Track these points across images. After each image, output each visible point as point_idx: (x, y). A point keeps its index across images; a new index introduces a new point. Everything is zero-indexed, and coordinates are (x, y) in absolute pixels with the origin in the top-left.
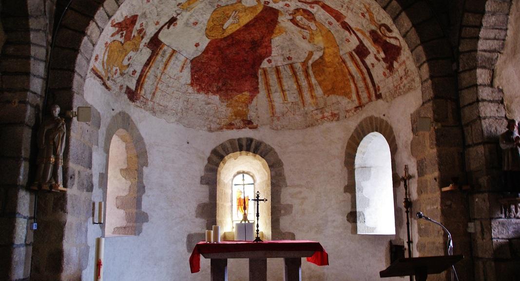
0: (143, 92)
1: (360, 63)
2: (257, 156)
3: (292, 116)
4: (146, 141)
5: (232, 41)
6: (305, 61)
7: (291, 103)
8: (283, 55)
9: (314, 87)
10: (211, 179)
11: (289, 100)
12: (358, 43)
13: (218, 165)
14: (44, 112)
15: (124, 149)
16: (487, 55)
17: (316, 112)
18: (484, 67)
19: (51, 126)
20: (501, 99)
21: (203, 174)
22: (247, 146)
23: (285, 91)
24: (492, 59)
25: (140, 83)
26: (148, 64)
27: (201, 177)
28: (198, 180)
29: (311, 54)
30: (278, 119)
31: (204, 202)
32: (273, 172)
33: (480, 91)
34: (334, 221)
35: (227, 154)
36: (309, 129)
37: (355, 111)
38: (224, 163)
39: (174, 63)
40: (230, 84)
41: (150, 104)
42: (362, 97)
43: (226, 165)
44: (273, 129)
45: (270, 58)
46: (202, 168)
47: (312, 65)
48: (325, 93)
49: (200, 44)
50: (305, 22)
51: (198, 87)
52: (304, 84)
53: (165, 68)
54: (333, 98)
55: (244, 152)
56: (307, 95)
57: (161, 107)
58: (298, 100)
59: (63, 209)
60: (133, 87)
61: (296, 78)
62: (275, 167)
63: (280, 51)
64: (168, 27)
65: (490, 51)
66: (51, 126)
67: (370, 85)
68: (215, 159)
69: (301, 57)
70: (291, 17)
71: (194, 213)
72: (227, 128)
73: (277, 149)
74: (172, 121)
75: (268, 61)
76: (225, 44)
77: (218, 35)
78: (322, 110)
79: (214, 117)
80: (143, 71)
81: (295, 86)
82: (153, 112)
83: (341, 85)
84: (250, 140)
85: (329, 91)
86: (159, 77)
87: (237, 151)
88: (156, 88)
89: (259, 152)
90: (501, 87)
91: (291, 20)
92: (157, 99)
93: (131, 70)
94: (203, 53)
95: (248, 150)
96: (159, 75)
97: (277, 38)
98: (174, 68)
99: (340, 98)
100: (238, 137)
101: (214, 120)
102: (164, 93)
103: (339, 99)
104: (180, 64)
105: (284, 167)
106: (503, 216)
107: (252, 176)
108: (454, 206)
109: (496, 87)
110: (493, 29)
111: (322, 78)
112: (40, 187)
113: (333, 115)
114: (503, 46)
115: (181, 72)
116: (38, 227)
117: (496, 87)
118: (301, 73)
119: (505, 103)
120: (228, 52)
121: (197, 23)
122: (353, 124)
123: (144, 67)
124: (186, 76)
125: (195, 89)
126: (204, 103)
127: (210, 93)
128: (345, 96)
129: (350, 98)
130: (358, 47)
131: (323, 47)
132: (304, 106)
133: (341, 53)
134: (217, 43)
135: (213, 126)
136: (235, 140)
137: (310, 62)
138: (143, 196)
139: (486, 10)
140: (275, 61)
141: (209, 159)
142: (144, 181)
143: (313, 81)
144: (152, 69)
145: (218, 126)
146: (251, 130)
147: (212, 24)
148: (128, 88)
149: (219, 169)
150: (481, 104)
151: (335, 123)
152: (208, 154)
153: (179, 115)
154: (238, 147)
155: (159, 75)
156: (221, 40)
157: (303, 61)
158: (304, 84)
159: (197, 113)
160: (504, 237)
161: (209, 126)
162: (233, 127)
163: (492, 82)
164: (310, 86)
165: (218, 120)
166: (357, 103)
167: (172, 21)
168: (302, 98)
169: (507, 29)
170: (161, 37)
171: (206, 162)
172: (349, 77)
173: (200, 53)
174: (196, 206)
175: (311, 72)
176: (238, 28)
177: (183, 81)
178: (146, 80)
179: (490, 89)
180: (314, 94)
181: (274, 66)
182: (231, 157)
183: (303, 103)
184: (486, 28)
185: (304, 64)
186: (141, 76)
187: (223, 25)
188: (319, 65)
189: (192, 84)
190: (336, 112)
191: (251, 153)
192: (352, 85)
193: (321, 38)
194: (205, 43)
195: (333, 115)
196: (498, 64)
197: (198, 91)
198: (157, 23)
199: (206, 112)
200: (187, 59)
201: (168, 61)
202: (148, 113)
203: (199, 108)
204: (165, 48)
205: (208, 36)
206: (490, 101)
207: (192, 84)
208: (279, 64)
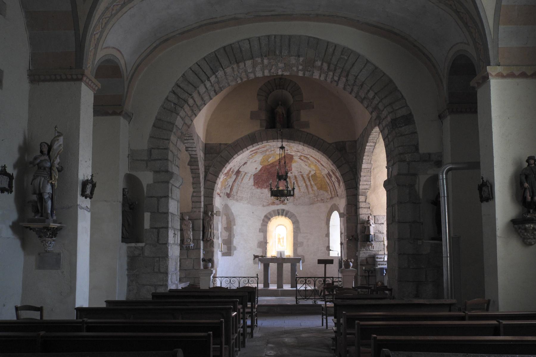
0: (233, 193)
1: (330, 179)
2: (287, 218)
4: (234, 214)
5: (273, 165)
6: (308, 174)
7: (303, 193)
8: (298, 171)
10: (264, 230)
11: (302, 191)
13: (267, 223)
14: (205, 213)
16: (364, 190)
18: (363, 195)
19: (209, 219)
20: (369, 207)
21: (260, 227)
22: (282, 213)
23: (299, 187)
24: (366, 192)
25: (231, 189)
28: (258, 230)
29: (310, 172)
31: (261, 240)
33: (361, 204)
37: (330, 199)
38: (270, 222)
39: (246, 178)
40: (273, 184)
41: (236, 197)
42: (332, 194)
43: (271, 222)
44: (294, 205)
45: (291, 171)
46: (260, 224)
48: (318, 189)
49: (258, 168)
50: (305, 159)
51: (257, 186)
52: (308, 184)
53: (242, 181)
54: (322, 192)
55: (280, 216)
56: (310, 189)
59: (213, 247)
64: (243, 166)
65: (365, 189)
66: (209, 219)
67: (335, 189)
68: (266, 220)
70: (299, 157)
71: (256, 246)
72: (272, 205)
73: (296, 214)
74: (245, 203)
75: (291, 173)
76: (269, 167)
79: (265, 199)
80: (232, 184)
81: (304, 185)
82: (237, 200)
84: (283, 210)
85: (319, 188)
87: (277, 216)
88: (238, 190)
89: (288, 216)
91: (299, 158)
92: (238, 195)
93: (228, 185)
94: (259, 171)
95: (282, 215)
97: (294, 164)
98: (246, 180)
99: (324, 192)
101: (265, 201)
102: (241, 191)
105: (299, 223)
106: (365, 250)
107: (285, 227)
109: (367, 202)
115: (249, 180)
117: (367, 202)
119: (370, 208)
120: (271, 170)
121: (256, 161)
122: (329, 206)
123: (233, 183)
124: (252, 182)
125: (256, 187)
126: (260, 193)
128: (326, 192)
129: (328, 193)
130: (328, 173)
132: (309, 194)
133: (323, 173)
135: (265, 204)
136: (276, 210)
137: (310, 175)
139: (362, 175)
140: (294, 173)
142: (234, 232)
143: (312, 183)
144: (236, 182)
146: (283, 205)
148: (227, 193)
149: (268, 225)
150: (360, 209)
152: (263, 217)
156: (268, 165)
158: (308, 184)
159: (257, 198)
161: (263, 204)
162: (275, 204)
163: (366, 200)
164: (311, 185)
165: (267, 201)
166: (330, 196)
168: (308, 190)
169: (371, 181)
170: (240, 170)
171: (262, 222)
172: (327, 184)
173: (258, 172)
174: (257, 243)
175: (311, 179)
176: (275, 160)
177: (250, 184)
178: (234, 187)
180: (313, 189)
181: (294, 175)
182: (274, 218)
183: (308, 192)
184: (362, 181)
185: (308, 175)
186: (232, 187)
187: (268, 160)
189: (254, 185)
190: (323, 199)
191: (284, 217)
192: (329, 188)
193: (313, 166)
194: (260, 167)
195: (322, 200)
196: (368, 194)
197: (257, 188)
199: (261, 197)
200: (252, 174)
202: (234, 202)
205: (261, 165)
206: (365, 208)
207: (254, 185)
208: (296, 174)
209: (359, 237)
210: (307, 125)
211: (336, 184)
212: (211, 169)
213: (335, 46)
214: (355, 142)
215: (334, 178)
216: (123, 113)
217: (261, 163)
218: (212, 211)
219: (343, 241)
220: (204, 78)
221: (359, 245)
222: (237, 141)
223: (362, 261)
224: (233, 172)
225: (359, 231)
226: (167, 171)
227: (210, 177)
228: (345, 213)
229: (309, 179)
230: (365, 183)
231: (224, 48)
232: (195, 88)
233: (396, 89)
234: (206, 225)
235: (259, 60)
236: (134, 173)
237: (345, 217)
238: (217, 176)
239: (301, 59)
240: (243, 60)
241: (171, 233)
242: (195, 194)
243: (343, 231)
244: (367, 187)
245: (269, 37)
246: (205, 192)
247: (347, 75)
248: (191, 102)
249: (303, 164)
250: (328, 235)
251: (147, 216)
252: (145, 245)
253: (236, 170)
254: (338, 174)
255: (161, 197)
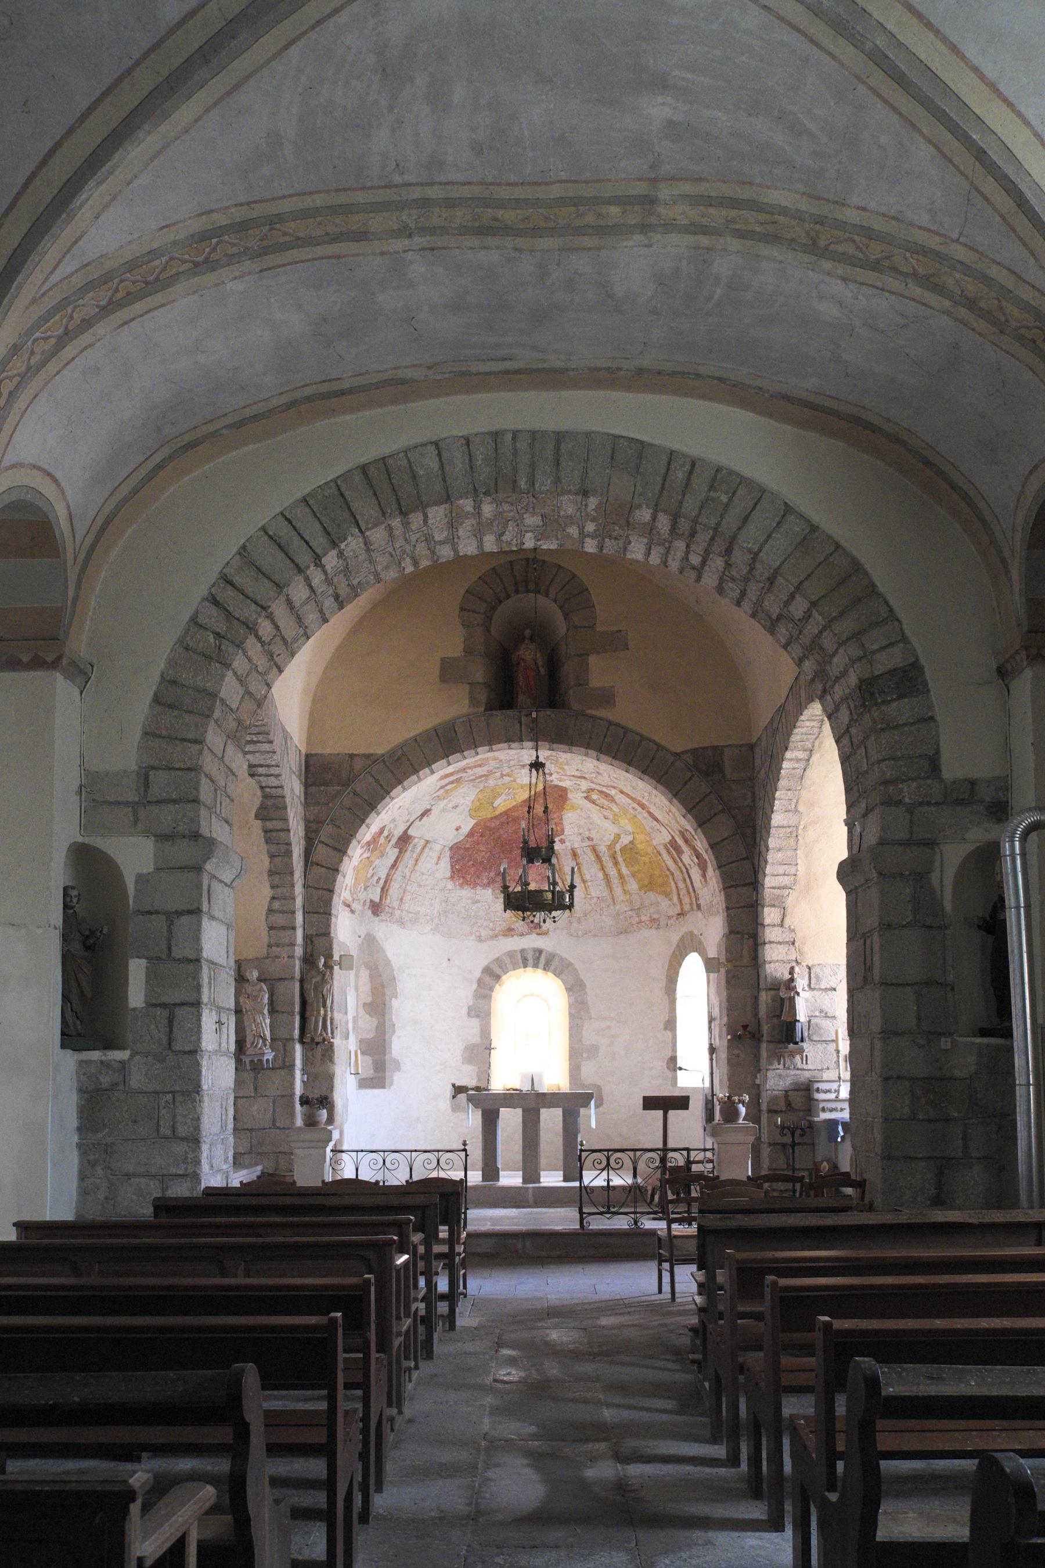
0: (388, 901)
2: (550, 974)
3: (599, 917)
7: (595, 899)
8: (580, 834)
9: (626, 878)
11: (593, 894)
12: (670, 838)
13: (491, 989)
14: (309, 960)
15: (368, 977)
17: (630, 912)
18: (774, 906)
19: (318, 979)
26: (394, 866)
27: (469, 1008)
28: (465, 1011)
30: (579, 920)
32: (572, 998)
34: (652, 1068)
35: (506, 973)
36: (622, 936)
37: (677, 919)
41: (397, 913)
44: (571, 935)
47: (620, 850)
48: (641, 888)
50: (602, 801)
51: (461, 881)
52: (613, 872)
53: (416, 864)
54: (652, 896)
56: (618, 891)
57: (410, 915)
58: (606, 893)
59: (331, 1060)
60: (377, 899)
61: (602, 865)
62: (575, 988)
63: (576, 829)
64: (420, 820)
66: (318, 979)
68: (487, 979)
69: (605, 839)
70: (585, 795)
71: (459, 1058)
77: (487, 814)
78: (638, 911)
80: (388, 875)
81: (601, 875)
82: (401, 922)
83: (660, 880)
86: (408, 877)
89: (552, 968)
90: (792, 927)
91: (586, 798)
94: (467, 836)
95: (536, 966)
96: (408, 874)
97: (570, 815)
98: (428, 862)
100: (520, 948)
103: (659, 899)
104: (435, 855)
106: (781, 1066)
108: (742, 1056)
110: (781, 864)
111: (635, 868)
112: (313, 1040)
113: (653, 920)
114: (795, 882)
115: (437, 864)
116: (308, 1079)
117: (787, 926)
118: (608, 858)
119: (797, 944)
120: (502, 831)
122: (675, 937)
124: (445, 867)
127: (478, 887)
130: (671, 841)
131: (631, 831)
132: (614, 904)
134: (485, 823)
135: (484, 933)
137: (618, 847)
138: (393, 1038)
140: (570, 841)
141: (480, 982)
143: (625, 871)
144: (399, 869)
145: (491, 933)
147: (478, 804)
148: (371, 901)
149: (494, 994)
151: (654, 932)
152: (477, 974)
153: (436, 921)
154: (520, 961)
155: (408, 874)
156: (492, 819)
157: (608, 843)
158: (613, 872)
160: (781, 1089)
161: (478, 934)
162: (513, 933)
163: (782, 921)
164: (621, 876)
165: (491, 924)
167: (426, 813)
171: (475, 986)
172: (668, 873)
173: (462, 838)
174: (462, 1048)
175: (620, 859)
177: (439, 875)
178: (393, 883)
179: (780, 930)
180: (626, 888)
185: (610, 847)
186: (386, 882)
187: (493, 803)
188: (630, 851)
189: (452, 878)
190: (655, 916)
193: (627, 821)
195: (653, 920)
197: (461, 886)
198: (408, 821)
199: (473, 913)
201: (420, 855)
202: (394, 927)
203: (463, 910)
204: (416, 840)
205: (472, 817)
207: (452, 878)
208: (576, 845)
209: (765, 1029)
210: (607, 698)
211: (696, 874)
212: (326, 832)
213: (693, 465)
214: (752, 747)
215: (687, 857)
216: (65, 661)
217: (472, 812)
218: (329, 956)
219: (717, 1043)
220: (304, 557)
221: (764, 1054)
222: (402, 746)
223: (774, 1099)
224: (388, 838)
225: (762, 1012)
226: (196, 836)
227: (321, 852)
228: (723, 960)
229: (614, 857)
230: (781, 870)
231: (364, 469)
232: (279, 587)
233: (872, 591)
234: (311, 995)
235: (467, 504)
236: (97, 842)
237: (723, 970)
238: (341, 850)
239: (593, 502)
240: (422, 506)
241: (208, 1020)
242: (276, 905)
243: (716, 1013)
244: (785, 881)
245: (496, 435)
246: (307, 899)
247: (729, 551)
248: (265, 629)
249: (596, 815)
250: (671, 1024)
251: (137, 970)
252: (132, 1056)
253: (398, 833)
254: (701, 844)
255: (179, 913)
